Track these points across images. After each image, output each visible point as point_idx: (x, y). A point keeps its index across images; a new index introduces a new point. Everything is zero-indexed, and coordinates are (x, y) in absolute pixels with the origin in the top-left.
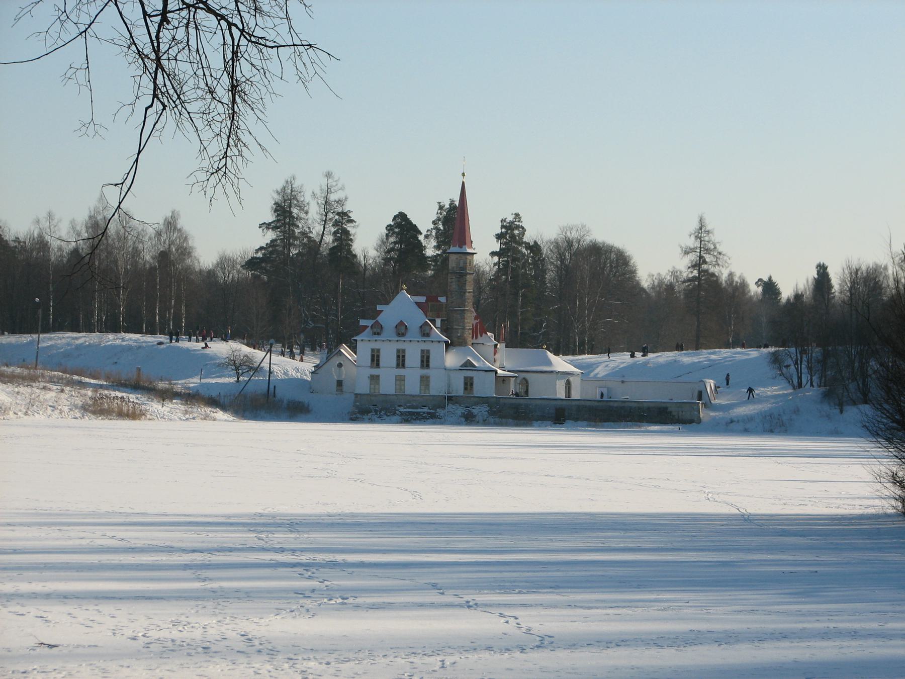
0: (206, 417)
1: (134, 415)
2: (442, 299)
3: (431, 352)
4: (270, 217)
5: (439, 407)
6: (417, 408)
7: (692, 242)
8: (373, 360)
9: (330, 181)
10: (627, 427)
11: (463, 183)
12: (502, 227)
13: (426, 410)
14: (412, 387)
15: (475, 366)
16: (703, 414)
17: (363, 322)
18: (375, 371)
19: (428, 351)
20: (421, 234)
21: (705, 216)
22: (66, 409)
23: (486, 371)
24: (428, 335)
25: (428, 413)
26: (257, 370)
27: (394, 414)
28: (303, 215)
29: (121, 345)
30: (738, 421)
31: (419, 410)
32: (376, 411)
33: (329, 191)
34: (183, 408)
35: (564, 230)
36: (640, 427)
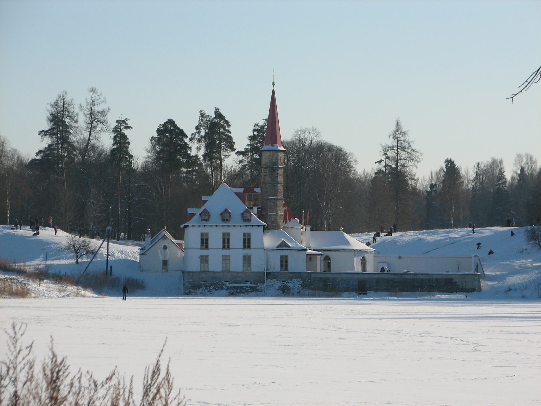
0: (77, 295)
1: (23, 294)
2: (258, 190)
4: (47, 126)
5: (260, 281)
6: (240, 283)
7: (391, 142)
8: (202, 243)
9: (94, 95)
11: (273, 91)
12: (254, 130)
13: (248, 284)
14: (236, 265)
15: (289, 246)
16: (484, 284)
17: (189, 211)
18: (205, 252)
19: (207, 234)
20: (187, 137)
23: (299, 250)
24: (249, 221)
25: (250, 287)
26: (94, 253)
27: (222, 288)
28: (73, 124)
30: (515, 290)
31: (243, 285)
32: (206, 286)
33: (93, 103)
34: (57, 286)
35: (298, 132)
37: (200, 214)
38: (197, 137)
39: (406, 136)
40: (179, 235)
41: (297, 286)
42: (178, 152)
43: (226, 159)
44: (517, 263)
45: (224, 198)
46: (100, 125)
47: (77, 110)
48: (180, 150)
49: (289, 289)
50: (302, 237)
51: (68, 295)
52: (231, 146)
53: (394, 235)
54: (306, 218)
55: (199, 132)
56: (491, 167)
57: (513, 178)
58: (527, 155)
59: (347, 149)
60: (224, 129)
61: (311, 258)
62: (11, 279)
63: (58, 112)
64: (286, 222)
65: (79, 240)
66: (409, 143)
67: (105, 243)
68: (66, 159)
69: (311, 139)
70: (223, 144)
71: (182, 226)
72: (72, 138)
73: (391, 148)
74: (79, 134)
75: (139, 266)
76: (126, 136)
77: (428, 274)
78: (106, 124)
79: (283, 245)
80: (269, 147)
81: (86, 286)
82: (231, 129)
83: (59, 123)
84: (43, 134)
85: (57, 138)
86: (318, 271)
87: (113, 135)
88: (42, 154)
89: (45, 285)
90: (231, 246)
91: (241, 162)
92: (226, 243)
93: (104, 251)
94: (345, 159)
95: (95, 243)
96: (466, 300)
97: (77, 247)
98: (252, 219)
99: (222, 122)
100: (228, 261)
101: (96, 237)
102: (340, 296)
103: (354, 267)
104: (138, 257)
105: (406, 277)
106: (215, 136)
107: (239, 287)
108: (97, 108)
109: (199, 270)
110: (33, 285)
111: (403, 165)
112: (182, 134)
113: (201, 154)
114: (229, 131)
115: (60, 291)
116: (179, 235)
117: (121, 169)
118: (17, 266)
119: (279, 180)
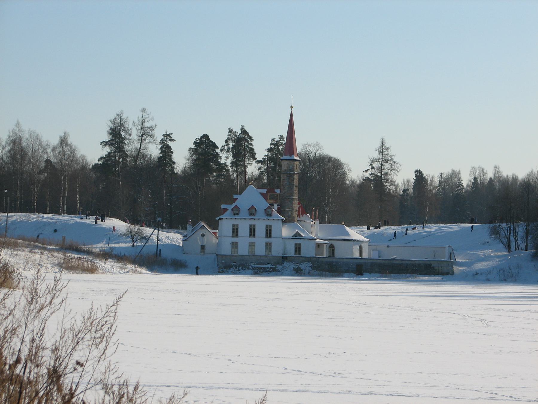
0: (135, 272)
1: (92, 270)
2: (278, 191)
3: (239, 226)
7: (377, 155)
8: (233, 232)
9: (144, 114)
10: (407, 278)
11: (291, 112)
12: (271, 144)
14: (260, 250)
15: (302, 236)
16: (456, 269)
17: (223, 206)
18: (235, 240)
21: (385, 138)
22: (49, 266)
23: (310, 239)
24: (270, 215)
25: (271, 268)
26: (147, 239)
27: (248, 268)
28: (128, 137)
29: (43, 222)
30: (481, 274)
33: (143, 121)
34: (120, 265)
36: (415, 277)
37: (232, 209)
38: (226, 148)
39: (389, 151)
40: (214, 225)
41: (308, 268)
42: (210, 160)
43: (249, 166)
44: (481, 253)
45: (251, 197)
46: (149, 138)
47: (130, 126)
48: (213, 159)
49: (302, 270)
50: (312, 229)
51: (128, 272)
52: (253, 156)
53: (382, 228)
54: (315, 213)
55: (228, 145)
56: (451, 176)
57: (468, 186)
58: (480, 168)
59: (343, 160)
60: (248, 142)
61: (319, 246)
62: (83, 258)
63: (116, 127)
64: (299, 217)
65: (136, 228)
66: (391, 156)
67: (156, 231)
68: (121, 164)
69: (314, 152)
70: (247, 155)
71: (217, 219)
72: (126, 148)
73: (377, 160)
74: (132, 145)
75: (182, 250)
77: (412, 260)
78: (154, 137)
79: (297, 235)
80: (287, 157)
81: (141, 265)
82: (253, 143)
83: (117, 135)
84: (104, 144)
85: (115, 147)
86: (325, 256)
88: (103, 160)
89: (109, 263)
90: (256, 235)
91: (259, 169)
92: (252, 232)
93: (154, 237)
94: (341, 168)
95: (147, 231)
96: (442, 281)
97: (133, 233)
98: (273, 214)
99: (247, 137)
100: (253, 247)
101: (177, 228)
102: (342, 276)
104: (181, 242)
105: (394, 262)
106: (241, 148)
107: (261, 267)
108: (146, 125)
109: (230, 254)
110: (100, 263)
111: (386, 174)
112: (215, 146)
113: (229, 162)
114: (251, 144)
115: (121, 268)
116: (214, 225)
117: (166, 172)
118: (86, 248)
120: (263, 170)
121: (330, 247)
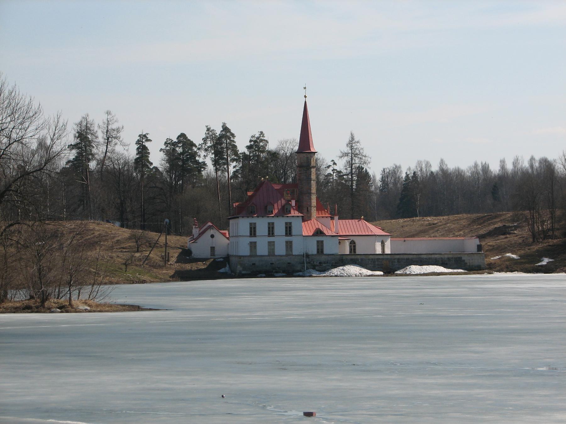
7: (347, 150)
11: (305, 102)
12: (251, 141)
19: (290, 223)
28: (95, 140)
35: (281, 143)
47: (96, 128)
58: (425, 160)
60: (229, 138)
76: (147, 148)
79: (319, 233)
82: (235, 140)
87: (136, 147)
90: (257, 234)
92: (271, 231)
99: (228, 134)
103: (374, 249)
108: (114, 126)
112: (192, 144)
114: (234, 141)
119: (312, 177)
120: (238, 168)
121: (351, 243)
